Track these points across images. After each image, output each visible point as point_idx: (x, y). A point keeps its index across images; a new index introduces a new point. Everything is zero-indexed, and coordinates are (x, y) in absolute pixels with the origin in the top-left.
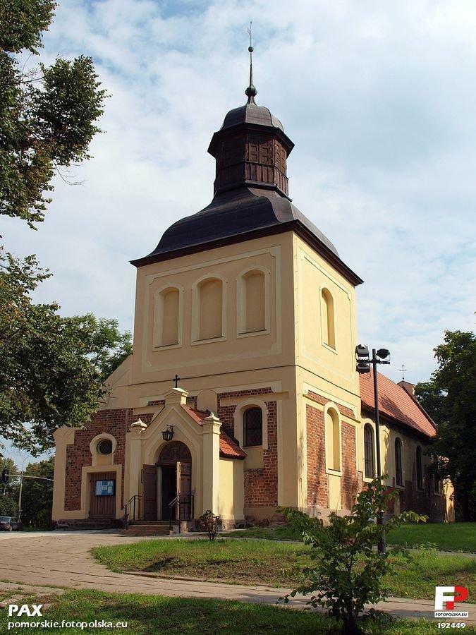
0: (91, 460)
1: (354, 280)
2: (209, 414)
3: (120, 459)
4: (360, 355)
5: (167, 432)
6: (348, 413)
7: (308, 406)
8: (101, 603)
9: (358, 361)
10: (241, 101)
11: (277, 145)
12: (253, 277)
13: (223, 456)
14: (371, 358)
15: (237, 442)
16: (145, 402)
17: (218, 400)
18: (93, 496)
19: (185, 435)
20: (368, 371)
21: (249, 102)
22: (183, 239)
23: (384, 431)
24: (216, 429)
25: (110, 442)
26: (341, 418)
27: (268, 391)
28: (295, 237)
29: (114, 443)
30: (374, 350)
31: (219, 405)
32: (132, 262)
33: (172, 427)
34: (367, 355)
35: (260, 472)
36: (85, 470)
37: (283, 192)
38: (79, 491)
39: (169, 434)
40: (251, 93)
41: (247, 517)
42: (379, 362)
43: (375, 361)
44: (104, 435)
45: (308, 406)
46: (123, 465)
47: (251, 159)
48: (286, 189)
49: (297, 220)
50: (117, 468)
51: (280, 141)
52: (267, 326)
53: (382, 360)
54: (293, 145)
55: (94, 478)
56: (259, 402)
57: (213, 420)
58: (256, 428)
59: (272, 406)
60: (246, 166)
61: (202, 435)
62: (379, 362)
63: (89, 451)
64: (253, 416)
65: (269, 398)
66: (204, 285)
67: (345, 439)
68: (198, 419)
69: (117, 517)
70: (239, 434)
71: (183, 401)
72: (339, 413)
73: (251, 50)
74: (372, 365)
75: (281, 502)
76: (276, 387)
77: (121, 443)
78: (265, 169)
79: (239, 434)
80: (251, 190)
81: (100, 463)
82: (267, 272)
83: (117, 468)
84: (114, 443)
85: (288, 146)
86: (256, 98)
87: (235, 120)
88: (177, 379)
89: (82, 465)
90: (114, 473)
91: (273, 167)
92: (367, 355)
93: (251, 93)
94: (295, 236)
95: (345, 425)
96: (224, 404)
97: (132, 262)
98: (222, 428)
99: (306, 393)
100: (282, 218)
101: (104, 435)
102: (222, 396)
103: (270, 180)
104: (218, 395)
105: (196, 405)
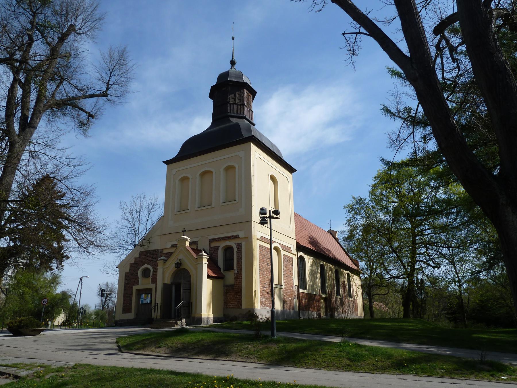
0: (138, 281)
1: (291, 170)
2: (201, 251)
3: (154, 281)
4: (262, 214)
5: (178, 263)
6: (287, 249)
7: (260, 246)
8: (94, 371)
9: (261, 217)
10: (227, 67)
11: (246, 92)
12: (229, 169)
13: (209, 277)
14: (268, 215)
15: (220, 269)
16: (169, 245)
17: (210, 243)
18: (140, 305)
19: (188, 265)
20: (266, 223)
21: (231, 68)
22: (194, 148)
23: (309, 260)
24: (205, 261)
25: (149, 270)
26: (283, 252)
27: (237, 237)
28: (252, 145)
29: (152, 271)
30: (270, 211)
31: (210, 246)
32: (165, 162)
33: (181, 260)
34: (266, 214)
35: (232, 286)
36: (135, 288)
37: (250, 120)
38: (131, 301)
39: (178, 265)
40: (233, 63)
41: (224, 315)
42: (273, 218)
43: (271, 217)
44: (146, 266)
45: (260, 246)
46: (156, 284)
47: (231, 101)
48: (252, 118)
49: (253, 136)
50: (153, 286)
51: (248, 90)
52: (237, 198)
53: (275, 216)
54: (256, 92)
55: (140, 292)
56: (232, 243)
57: (203, 255)
58: (230, 262)
59: (239, 246)
60: (228, 105)
61: (197, 264)
62: (273, 218)
63: (137, 276)
64: (228, 250)
65: (237, 241)
66: (204, 174)
67: (285, 265)
68: (194, 255)
69: (153, 317)
70: (221, 263)
71: (188, 244)
72: (281, 249)
73: (233, 39)
74: (269, 219)
75: (244, 306)
76: (241, 234)
77: (155, 271)
78: (239, 107)
79: (221, 263)
80: (231, 119)
81: (143, 283)
82: (236, 166)
83: (153, 286)
84: (152, 271)
85: (254, 93)
86: (235, 66)
87: (223, 78)
88: (184, 231)
89: (134, 285)
90: (151, 289)
91: (243, 105)
92: (266, 214)
93: (233, 63)
94: (252, 145)
95: (286, 257)
96: (214, 245)
97: (165, 162)
98: (209, 261)
99: (259, 237)
100: (245, 135)
101: (146, 266)
102: (212, 241)
103: (242, 113)
104: (210, 240)
105: (197, 246)
